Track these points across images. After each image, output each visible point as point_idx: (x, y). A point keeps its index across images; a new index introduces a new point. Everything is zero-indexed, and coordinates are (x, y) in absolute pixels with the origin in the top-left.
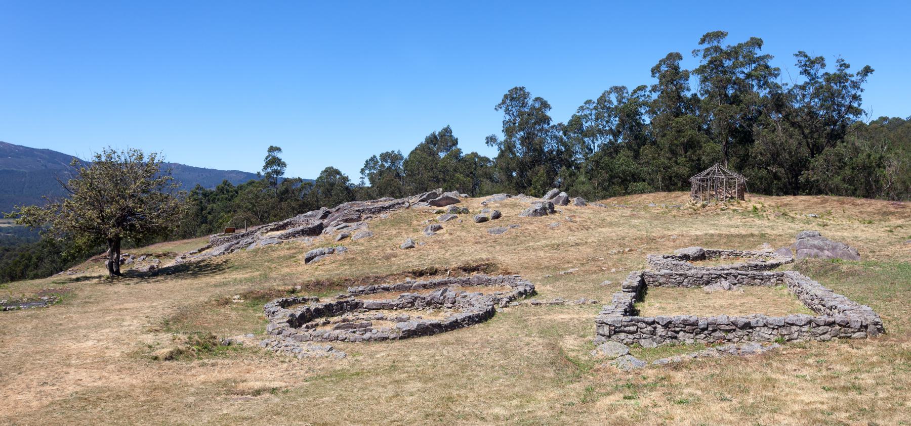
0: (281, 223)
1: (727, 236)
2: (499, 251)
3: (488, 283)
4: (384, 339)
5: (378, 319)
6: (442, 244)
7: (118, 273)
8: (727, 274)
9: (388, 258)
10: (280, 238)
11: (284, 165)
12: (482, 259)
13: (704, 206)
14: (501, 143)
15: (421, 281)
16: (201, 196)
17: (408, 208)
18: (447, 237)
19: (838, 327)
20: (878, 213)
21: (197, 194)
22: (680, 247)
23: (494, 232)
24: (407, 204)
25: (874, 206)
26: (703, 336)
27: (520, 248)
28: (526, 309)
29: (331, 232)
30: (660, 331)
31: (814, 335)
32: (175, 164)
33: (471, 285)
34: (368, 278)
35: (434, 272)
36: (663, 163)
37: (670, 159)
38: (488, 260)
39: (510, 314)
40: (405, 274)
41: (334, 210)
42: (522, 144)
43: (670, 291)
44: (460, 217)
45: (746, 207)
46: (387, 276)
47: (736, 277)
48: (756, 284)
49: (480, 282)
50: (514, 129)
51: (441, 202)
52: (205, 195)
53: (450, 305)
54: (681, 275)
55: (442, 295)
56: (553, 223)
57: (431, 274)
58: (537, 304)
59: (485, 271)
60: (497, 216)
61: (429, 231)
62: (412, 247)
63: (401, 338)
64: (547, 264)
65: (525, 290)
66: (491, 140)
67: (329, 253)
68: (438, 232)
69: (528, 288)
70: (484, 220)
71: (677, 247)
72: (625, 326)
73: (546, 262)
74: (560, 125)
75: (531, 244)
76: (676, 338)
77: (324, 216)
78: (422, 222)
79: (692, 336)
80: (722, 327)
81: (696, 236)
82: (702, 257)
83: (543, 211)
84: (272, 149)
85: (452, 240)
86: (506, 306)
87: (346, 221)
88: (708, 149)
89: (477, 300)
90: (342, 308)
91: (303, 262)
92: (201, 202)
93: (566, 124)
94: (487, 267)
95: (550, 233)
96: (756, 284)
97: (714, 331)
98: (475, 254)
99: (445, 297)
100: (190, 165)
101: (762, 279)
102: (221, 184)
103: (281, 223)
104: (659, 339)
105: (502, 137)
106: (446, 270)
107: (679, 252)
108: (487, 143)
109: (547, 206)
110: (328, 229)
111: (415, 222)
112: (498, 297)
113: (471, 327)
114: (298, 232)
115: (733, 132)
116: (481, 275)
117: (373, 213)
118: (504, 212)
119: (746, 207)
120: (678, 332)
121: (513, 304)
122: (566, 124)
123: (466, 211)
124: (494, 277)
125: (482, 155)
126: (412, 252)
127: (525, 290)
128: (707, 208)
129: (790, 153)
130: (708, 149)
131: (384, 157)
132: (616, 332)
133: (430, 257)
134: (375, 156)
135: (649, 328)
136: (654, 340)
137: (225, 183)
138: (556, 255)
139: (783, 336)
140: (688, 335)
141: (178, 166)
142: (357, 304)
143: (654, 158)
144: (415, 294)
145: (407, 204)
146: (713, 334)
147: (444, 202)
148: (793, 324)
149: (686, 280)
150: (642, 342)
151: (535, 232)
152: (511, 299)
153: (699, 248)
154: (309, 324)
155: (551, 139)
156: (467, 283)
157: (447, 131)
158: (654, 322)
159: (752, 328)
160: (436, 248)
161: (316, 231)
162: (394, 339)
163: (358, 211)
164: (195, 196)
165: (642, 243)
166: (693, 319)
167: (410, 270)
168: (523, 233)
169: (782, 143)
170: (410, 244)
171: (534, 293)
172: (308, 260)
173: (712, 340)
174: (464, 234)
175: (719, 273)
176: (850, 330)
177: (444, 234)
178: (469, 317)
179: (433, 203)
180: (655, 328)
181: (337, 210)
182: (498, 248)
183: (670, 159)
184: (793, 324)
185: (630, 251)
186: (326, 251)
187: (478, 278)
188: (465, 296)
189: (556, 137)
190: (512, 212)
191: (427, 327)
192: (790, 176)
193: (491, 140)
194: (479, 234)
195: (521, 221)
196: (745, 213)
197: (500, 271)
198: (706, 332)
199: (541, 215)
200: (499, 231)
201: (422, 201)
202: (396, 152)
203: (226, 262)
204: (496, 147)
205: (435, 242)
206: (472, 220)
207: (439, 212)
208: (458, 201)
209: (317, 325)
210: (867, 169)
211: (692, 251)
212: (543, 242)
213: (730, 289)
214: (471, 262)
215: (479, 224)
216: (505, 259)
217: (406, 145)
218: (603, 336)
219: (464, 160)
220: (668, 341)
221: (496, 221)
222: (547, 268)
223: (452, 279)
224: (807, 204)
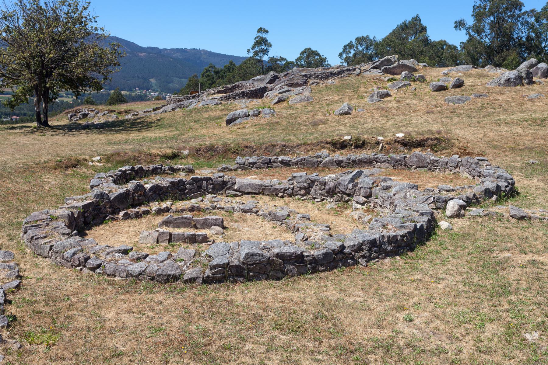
0: (229, 86)
2: (458, 123)
3: (433, 166)
4: (170, 279)
5: (245, 211)
6: (386, 113)
7: (46, 124)
9: (315, 124)
10: (220, 99)
11: (270, 45)
12: (431, 132)
14: (469, 28)
15: (338, 156)
16: (213, 73)
17: (358, 75)
18: (394, 104)
21: (209, 71)
23: (453, 101)
24: (358, 71)
27: (487, 121)
28: (499, 227)
29: (272, 95)
32: (203, 50)
33: (408, 167)
34: (274, 146)
35: (360, 145)
38: (439, 132)
39: (465, 236)
40: (321, 144)
41: (282, 74)
42: (491, 29)
44: (414, 85)
46: (299, 146)
49: (422, 164)
50: (484, 13)
51: (395, 70)
52: (217, 72)
53: (362, 199)
55: (352, 180)
56: (533, 95)
57: (357, 147)
58: (522, 218)
59: (433, 148)
60: (459, 85)
61: (375, 98)
62: (347, 113)
63: (207, 281)
64: (530, 145)
65: (498, 187)
66: (459, 24)
67: (253, 116)
68: (385, 99)
69: (502, 183)
70: (441, 88)
73: (526, 141)
74: (532, 11)
75: (502, 117)
77: (272, 81)
78: (370, 89)
83: (518, 81)
84: (260, 30)
85: (398, 108)
86: (458, 215)
87: (291, 85)
89: (403, 201)
90: (199, 188)
91: (225, 124)
92: (213, 78)
93: (539, 10)
94: (437, 143)
95: (529, 105)
98: (422, 124)
99: (356, 185)
100: (215, 52)
102: (228, 64)
103: (229, 86)
105: (470, 21)
106: (378, 143)
108: (456, 27)
109: (524, 75)
110: (269, 93)
111: (362, 89)
112: (445, 195)
113: (375, 264)
114: (238, 95)
116: (428, 155)
117: (321, 79)
118: (468, 82)
121: (474, 211)
122: (539, 10)
123: (422, 79)
124: (443, 158)
125: (451, 43)
126: (346, 120)
127: (498, 187)
131: (360, 40)
133: (365, 126)
134: (351, 42)
137: (231, 63)
138: (541, 133)
141: (206, 52)
142: (224, 183)
144: (313, 176)
145: (358, 71)
147: (399, 70)
151: (508, 103)
152: (470, 202)
154: (132, 211)
155: (522, 24)
156: (401, 165)
157: (417, 19)
160: (376, 116)
161: (259, 93)
162: (192, 280)
163: (305, 76)
164: (208, 73)
167: (329, 140)
168: (491, 104)
170: (346, 109)
171: (512, 192)
172: (229, 122)
174: (415, 102)
177: (390, 102)
178: (373, 243)
179: (386, 71)
181: (285, 75)
182: (456, 120)
186: (251, 113)
187: (419, 157)
188: (388, 188)
189: (527, 23)
190: (478, 82)
191: (269, 261)
193: (459, 24)
194: (434, 103)
195: (489, 90)
197: (455, 149)
199: (516, 85)
200: (460, 100)
201: (375, 68)
202: (371, 38)
203: (158, 120)
204: (464, 31)
205: (377, 109)
206: (427, 89)
207: (390, 80)
208: (415, 70)
209: (147, 213)
212: (520, 116)
214: (414, 134)
215: (436, 93)
216: (464, 133)
217: (380, 32)
219: (433, 45)
221: (457, 90)
222: (530, 149)
223: (380, 155)
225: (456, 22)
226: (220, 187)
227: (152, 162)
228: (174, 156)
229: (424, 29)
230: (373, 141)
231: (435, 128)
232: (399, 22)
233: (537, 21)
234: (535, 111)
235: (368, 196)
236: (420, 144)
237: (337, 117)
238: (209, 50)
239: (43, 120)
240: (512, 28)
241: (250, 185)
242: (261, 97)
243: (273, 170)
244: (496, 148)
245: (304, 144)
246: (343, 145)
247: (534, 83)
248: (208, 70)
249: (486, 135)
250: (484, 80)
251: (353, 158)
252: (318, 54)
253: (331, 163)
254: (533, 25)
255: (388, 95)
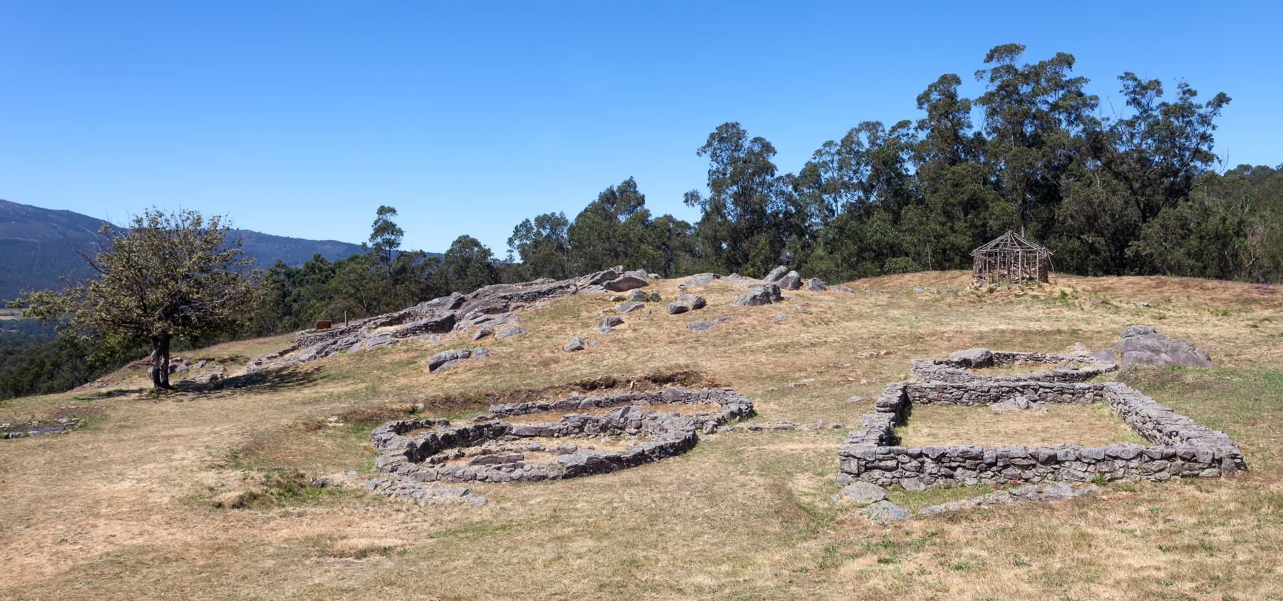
0: (396, 315)
1: (1024, 333)
2: (703, 354)
3: (687, 399)
4: (541, 478)
5: (533, 450)
6: (623, 344)
7: (166, 385)
8: (1023, 387)
9: (546, 364)
10: (395, 335)
11: (401, 232)
12: (678, 366)
13: (991, 291)
14: (705, 202)
15: (593, 396)
16: (282, 277)
17: (574, 293)
18: (629, 334)
19: (1180, 462)
20: (1237, 301)
21: (278, 273)
22: (958, 348)
23: (695, 327)
24: (573, 288)
25: (1231, 291)
26: (990, 473)
27: (733, 349)
28: (741, 436)
29: (466, 327)
30: (930, 466)
31: (1147, 472)
32: (246, 231)
33: (663, 401)
34: (519, 392)
35: (611, 384)
36: (934, 230)
37: (943, 225)
38: (687, 366)
39: (718, 443)
40: (570, 386)
41: (470, 296)
42: (735, 203)
43: (943, 410)
44: (648, 306)
45: (1051, 293)
46: (545, 389)
47: (1036, 391)
48: (1064, 401)
49: (676, 398)
50: (724, 181)
51: (621, 286)
52: (289, 275)
53: (634, 431)
54: (959, 388)
55: (622, 416)
56: (779, 315)
57: (607, 387)
58: (756, 429)
59: (682, 382)
60: (700, 305)
61: (604, 326)
62: (580, 348)
63: (565, 477)
64: (771, 372)
65: (740, 410)
66: (691, 198)
67: (464, 357)
68: (617, 327)
69: (743, 407)
70: (681, 310)
71: (953, 349)
72: (880, 460)
73: (769, 370)
74: (789, 176)
75: (748, 344)
76: (952, 476)
77: (457, 305)
78: (595, 313)
79: (974, 474)
80: (1017, 461)
81: (981, 332)
82: (988, 362)
83: (765, 298)
84: (382, 210)
85: (636, 338)
86: (712, 432)
87: (487, 311)
88: (997, 211)
89: (671, 423)
90: (481, 434)
91: (427, 370)
92: (283, 285)
93: (797, 174)
94: (685, 377)
95: (775, 328)
96: (1064, 401)
97: (1006, 467)
98: (669, 358)
99: (626, 419)
100: (268, 233)
101: (1073, 394)
102: (311, 260)
103: (396, 315)
104: (928, 478)
105: (706, 193)
106: (629, 381)
107: (956, 356)
108: (686, 201)
109: (770, 290)
110: (462, 323)
111: (584, 314)
112: (702, 419)
113: (664, 461)
114: (420, 328)
115: (1032, 186)
116: (678, 388)
117: (526, 300)
118: (710, 300)
119: (1051, 293)
120: (954, 469)
121: (722, 428)
122: (797, 174)
123: (656, 298)
124: (695, 391)
125: (679, 219)
126: (580, 356)
127: (740, 410)
128: (996, 293)
129: (1113, 216)
130: (997, 211)
131: (541, 221)
132: (867, 469)
133: (605, 363)
134: (527, 221)
135: (915, 463)
136: (921, 480)
137: (317, 258)
138: (783, 360)
139: (1103, 474)
140: (969, 472)
141: (251, 234)
142: (503, 429)
143: (921, 223)
144: (585, 415)
145: (573, 288)
146: (1004, 471)
147: (625, 285)
148: (1116, 458)
149: (966, 395)
150: (905, 482)
151: (754, 327)
152: (720, 422)
153: (984, 350)
154: (435, 457)
155: (776, 196)
156: (658, 400)
157: (630, 185)
158: (921, 455)
159: (1058, 462)
160: (614, 350)
161: (445, 326)
162: (554, 478)
163: (505, 297)
164: (275, 277)
165: (905, 343)
166: (976, 450)
167: (578, 381)
168: (736, 328)
169: (1101, 202)
170: (578, 344)
171: (751, 414)
172: (433, 367)
173: (1002, 480)
174: (653, 329)
175: (1012, 385)
176: (1198, 466)
177: (625, 330)
178: (661, 447)
179: (610, 287)
180: (923, 463)
181: (475, 297)
182: (701, 349)
183: (943, 225)
184: (1116, 458)
185: (887, 354)
186: (460, 354)
187: (674, 392)
188: (655, 418)
189: (783, 193)
190: (721, 299)
191: (602, 462)
192: (1113, 249)
193: (691, 198)
194: (675, 331)
195: (734, 312)
196: (1049, 300)
197: (704, 382)
198: (994, 468)
199: (762, 303)
200: (703, 326)
201: (595, 283)
202: (557, 215)
203: (318, 370)
204: (698, 208)
205: (613, 341)
206: (664, 311)
207: (618, 300)
208: (645, 284)
209: (446, 458)
210: (1221, 238)
211: (975, 354)
212: (765, 342)
213: (1028, 408)
214: (663, 370)
215: (675, 316)
216: (711, 365)
217: (571, 205)
218: (850, 473)
219: (653, 226)
220: (941, 481)
221: (699, 311)
222: (771, 378)
223: (636, 393)
224: (1136, 288)
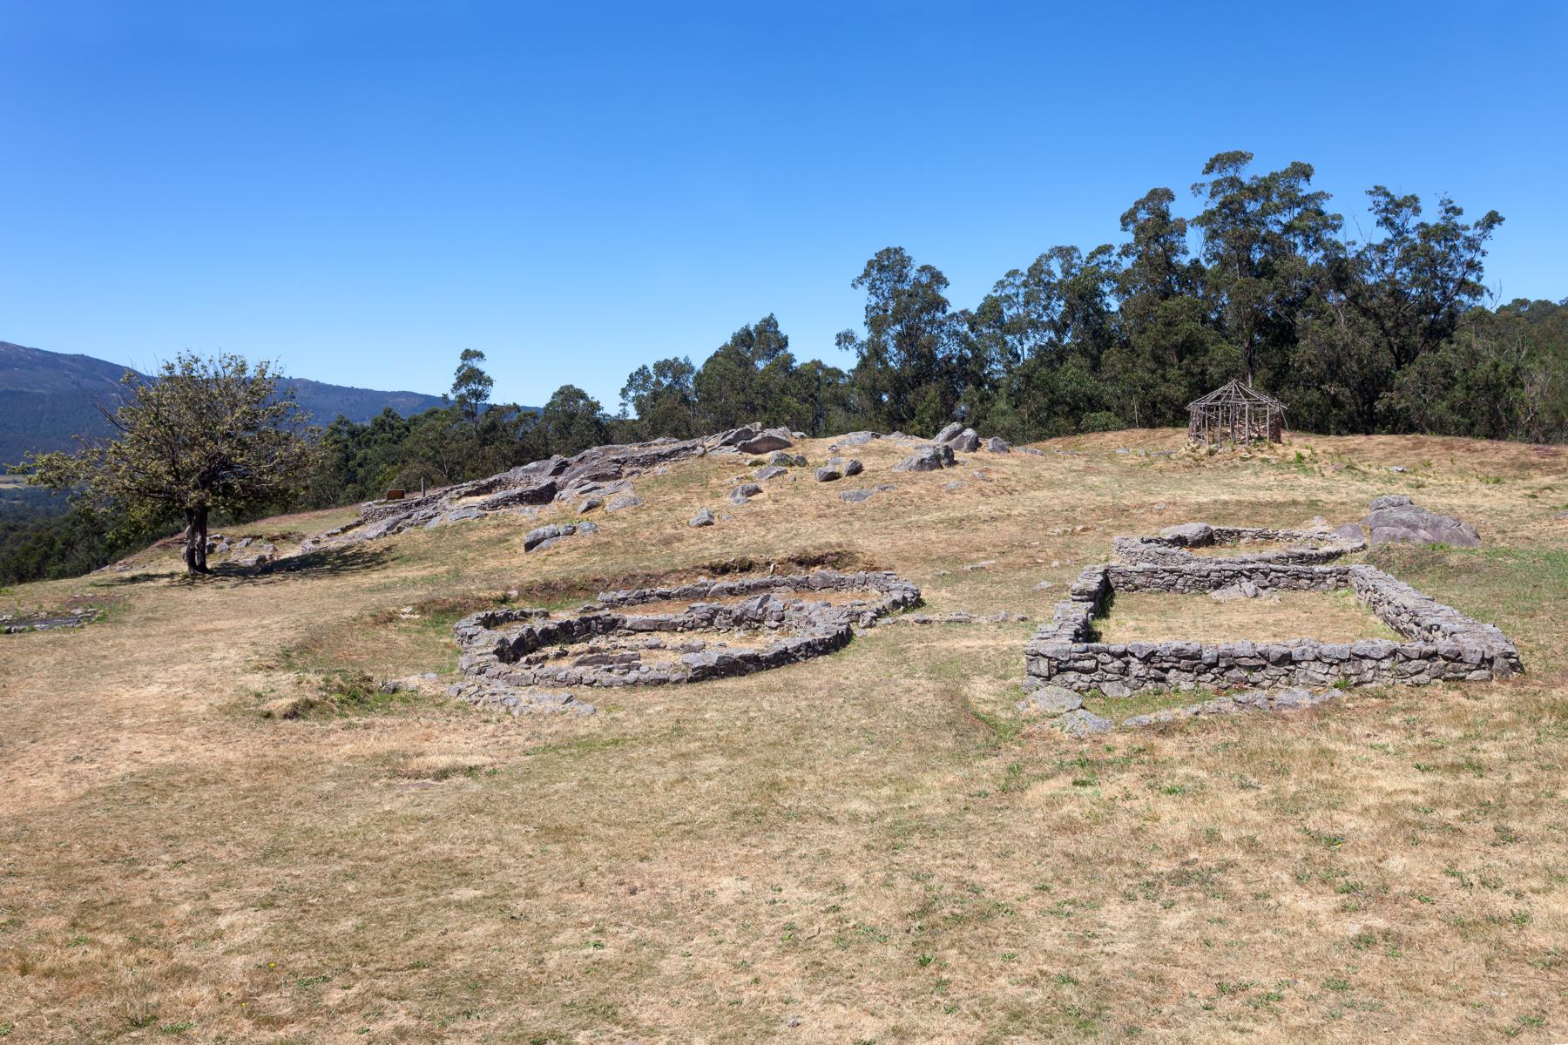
0: (484, 482)
3: (840, 585)
4: (661, 682)
5: (651, 648)
7: (202, 568)
8: (1250, 570)
9: (667, 542)
10: (482, 507)
11: (490, 382)
12: (829, 545)
13: (1211, 453)
14: (862, 345)
15: (725, 582)
16: (345, 436)
17: (702, 456)
18: (769, 506)
19: (1442, 662)
20: (1512, 465)
21: (340, 432)
24: (700, 450)
26: (1210, 676)
27: (896, 524)
28: (905, 630)
29: (570, 497)
30: (1136, 667)
31: (1402, 675)
32: (300, 380)
33: (811, 588)
35: (747, 567)
36: (1141, 379)
38: (840, 545)
39: (878, 639)
40: (697, 570)
41: (575, 459)
42: (899, 346)
43: (1153, 599)
44: (792, 472)
47: (1266, 575)
48: (1300, 588)
50: (885, 319)
51: (758, 447)
52: (353, 434)
54: (1172, 572)
55: (760, 606)
56: (952, 483)
57: (742, 570)
58: (924, 622)
59: (834, 565)
60: (856, 470)
61: (739, 496)
62: (708, 523)
63: (691, 681)
65: (904, 598)
66: (845, 339)
68: (754, 498)
69: (909, 595)
70: (832, 477)
72: (1076, 660)
73: (939, 550)
74: (964, 312)
75: (914, 518)
76: (1163, 680)
77: (558, 471)
78: (727, 481)
80: (1243, 661)
82: (1208, 540)
83: (935, 462)
84: (467, 355)
85: (777, 512)
86: (871, 626)
87: (596, 478)
88: (1219, 355)
89: (820, 615)
90: (588, 628)
91: (522, 550)
93: (974, 311)
94: (838, 558)
97: (1229, 668)
98: (817, 535)
102: (380, 415)
103: (484, 482)
104: (1134, 681)
105: (863, 334)
106: (768, 564)
107: (1168, 533)
108: (839, 344)
109: (942, 453)
110: (564, 493)
111: (714, 481)
112: (858, 609)
114: (513, 498)
115: (1261, 325)
117: (643, 465)
118: (868, 464)
120: (1166, 671)
121: (883, 621)
122: (974, 311)
123: (802, 462)
124: (849, 576)
126: (709, 533)
127: (904, 598)
128: (1217, 456)
129: (1360, 361)
130: (1219, 355)
132: (1060, 671)
133: (739, 541)
134: (645, 367)
135: (1118, 663)
136: (1125, 684)
137: (388, 413)
138: (957, 537)
139: (1348, 676)
141: (307, 384)
142: (615, 621)
143: (1126, 371)
144: (715, 604)
145: (700, 450)
148: (1364, 657)
150: (1106, 687)
152: (880, 614)
153: (1203, 525)
154: (532, 656)
155: (949, 337)
156: (804, 586)
157: (769, 324)
158: (1125, 653)
159: (1294, 663)
160: (751, 525)
161: (544, 495)
162: (677, 682)
163: (617, 461)
164: (336, 436)
165: (1106, 517)
166: (1192, 649)
169: (1346, 345)
171: (918, 603)
172: (529, 546)
173: (1225, 684)
174: (798, 500)
175: (1237, 568)
177: (763, 501)
178: (808, 644)
179: (745, 448)
180: (1128, 663)
181: (580, 460)
182: (857, 525)
183: (1153, 372)
184: (1364, 657)
185: (1084, 530)
186: (562, 531)
187: (824, 577)
188: (801, 609)
189: (956, 333)
190: (882, 463)
191: (735, 662)
192: (1360, 402)
193: (845, 339)
196: (1282, 465)
197: (860, 565)
198: (1215, 670)
199: (932, 468)
200: (859, 496)
201: (727, 444)
202: (681, 360)
204: (853, 351)
205: (749, 514)
206: (812, 478)
207: (755, 464)
209: (546, 658)
210: (1493, 389)
211: (1191, 530)
212: (936, 515)
213: (1256, 596)
214: (810, 549)
216: (870, 543)
219: (798, 374)
220: (1150, 686)
221: (854, 478)
222: (942, 559)
223: (777, 578)
224: (1389, 449)
225: (839, 336)
226: (611, 626)
227: (484, 608)
228: (505, 600)
229: (784, 343)
230: (762, 561)
231: (834, 538)
232: (737, 328)
233: (972, 329)
234: (954, 508)
235: (780, 620)
236: (819, 561)
237: (695, 531)
238: (349, 385)
239: (197, 562)
240: (933, 342)
241: (644, 622)
242: (550, 499)
243: (651, 606)
244: (906, 559)
245: (674, 571)
246: (725, 570)
247: (956, 463)
248: (336, 430)
249: (894, 545)
250: (890, 461)
251: (747, 583)
252: (582, 395)
253: (721, 591)
254: (966, 337)
255: (757, 491)
